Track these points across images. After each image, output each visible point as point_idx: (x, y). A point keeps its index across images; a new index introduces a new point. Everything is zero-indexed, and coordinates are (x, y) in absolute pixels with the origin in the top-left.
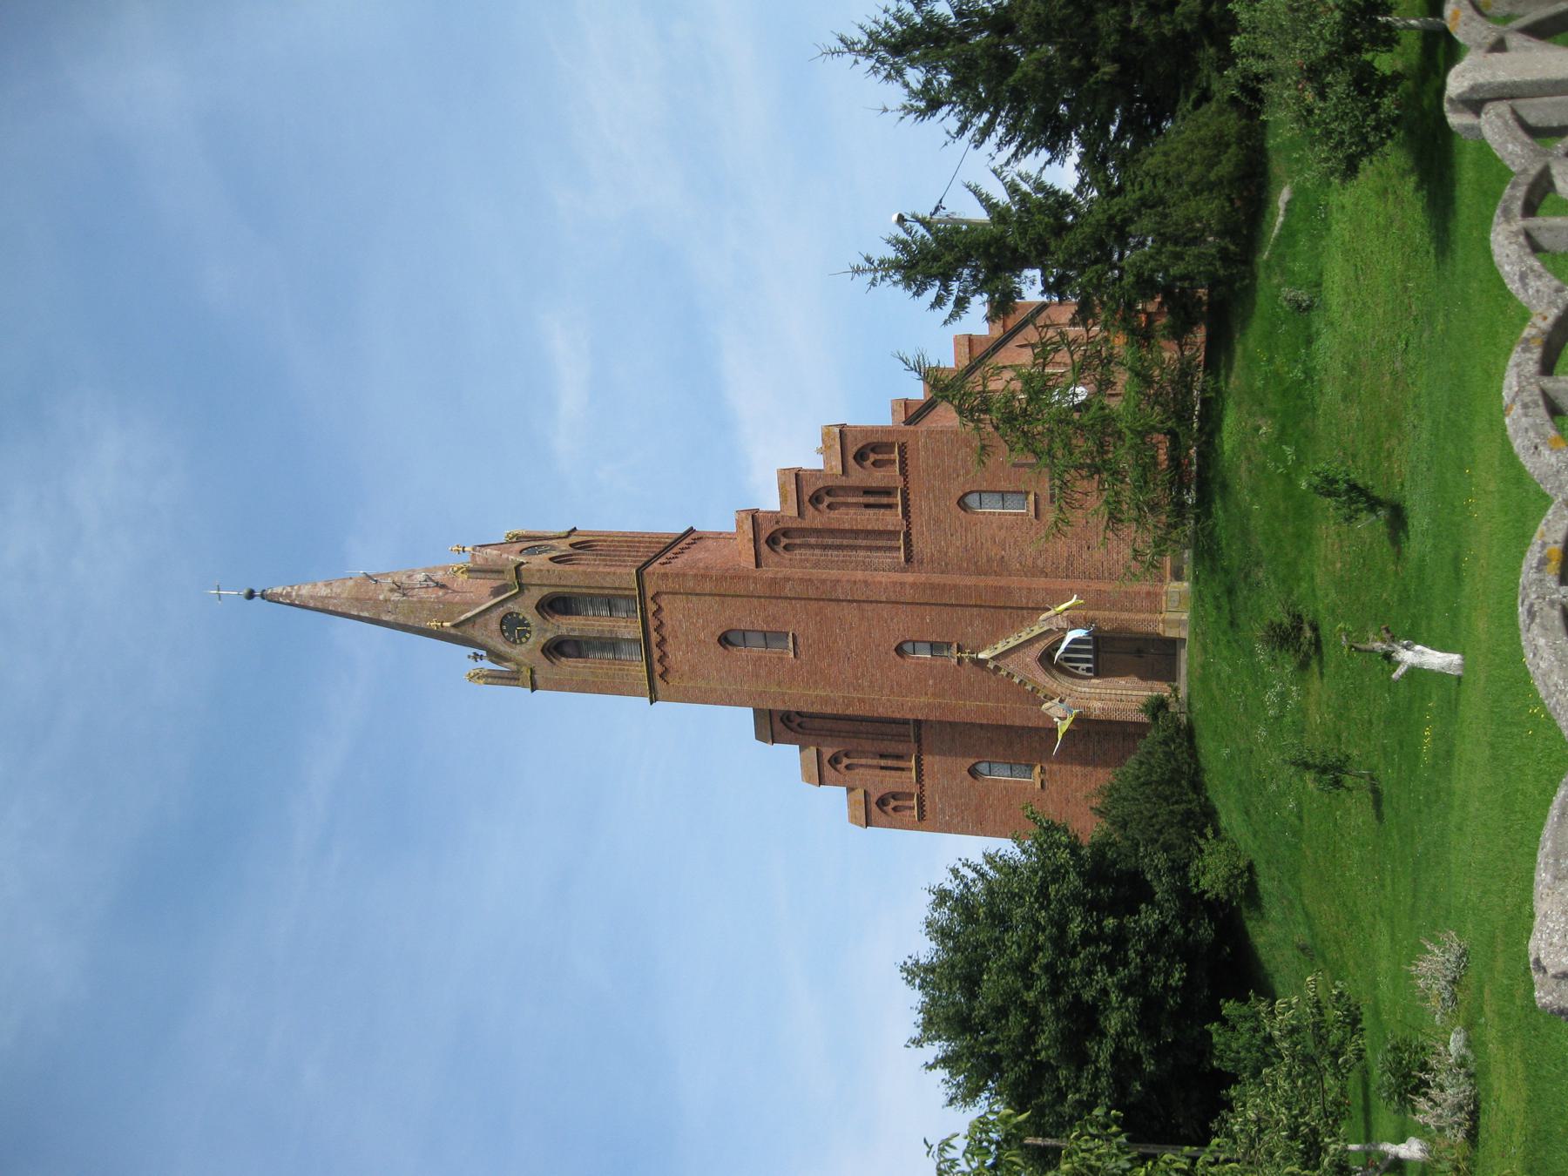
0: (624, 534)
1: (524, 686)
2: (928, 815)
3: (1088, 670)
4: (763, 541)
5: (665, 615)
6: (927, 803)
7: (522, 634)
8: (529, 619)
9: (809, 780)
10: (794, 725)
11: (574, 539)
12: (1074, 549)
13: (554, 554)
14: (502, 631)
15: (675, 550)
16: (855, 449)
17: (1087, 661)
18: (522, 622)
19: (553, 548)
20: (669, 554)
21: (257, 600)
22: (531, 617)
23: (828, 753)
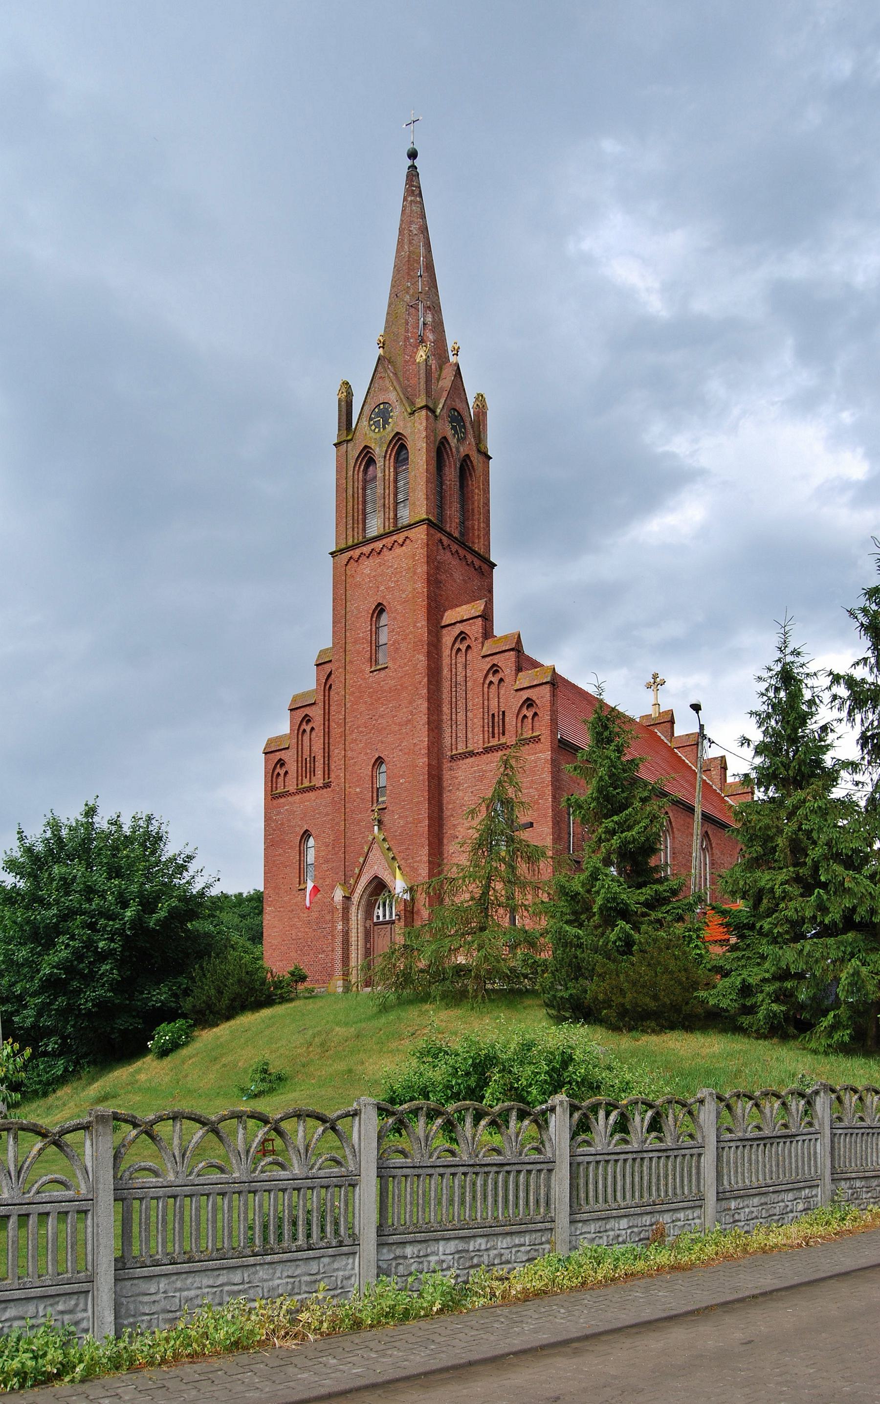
1: (339, 436)
2: (275, 802)
3: (378, 917)
4: (462, 628)
5: (398, 551)
7: (377, 424)
9: (294, 700)
11: (476, 458)
15: (462, 552)
16: (534, 698)
17: (384, 916)
18: (386, 422)
21: (409, 162)
23: (313, 712)
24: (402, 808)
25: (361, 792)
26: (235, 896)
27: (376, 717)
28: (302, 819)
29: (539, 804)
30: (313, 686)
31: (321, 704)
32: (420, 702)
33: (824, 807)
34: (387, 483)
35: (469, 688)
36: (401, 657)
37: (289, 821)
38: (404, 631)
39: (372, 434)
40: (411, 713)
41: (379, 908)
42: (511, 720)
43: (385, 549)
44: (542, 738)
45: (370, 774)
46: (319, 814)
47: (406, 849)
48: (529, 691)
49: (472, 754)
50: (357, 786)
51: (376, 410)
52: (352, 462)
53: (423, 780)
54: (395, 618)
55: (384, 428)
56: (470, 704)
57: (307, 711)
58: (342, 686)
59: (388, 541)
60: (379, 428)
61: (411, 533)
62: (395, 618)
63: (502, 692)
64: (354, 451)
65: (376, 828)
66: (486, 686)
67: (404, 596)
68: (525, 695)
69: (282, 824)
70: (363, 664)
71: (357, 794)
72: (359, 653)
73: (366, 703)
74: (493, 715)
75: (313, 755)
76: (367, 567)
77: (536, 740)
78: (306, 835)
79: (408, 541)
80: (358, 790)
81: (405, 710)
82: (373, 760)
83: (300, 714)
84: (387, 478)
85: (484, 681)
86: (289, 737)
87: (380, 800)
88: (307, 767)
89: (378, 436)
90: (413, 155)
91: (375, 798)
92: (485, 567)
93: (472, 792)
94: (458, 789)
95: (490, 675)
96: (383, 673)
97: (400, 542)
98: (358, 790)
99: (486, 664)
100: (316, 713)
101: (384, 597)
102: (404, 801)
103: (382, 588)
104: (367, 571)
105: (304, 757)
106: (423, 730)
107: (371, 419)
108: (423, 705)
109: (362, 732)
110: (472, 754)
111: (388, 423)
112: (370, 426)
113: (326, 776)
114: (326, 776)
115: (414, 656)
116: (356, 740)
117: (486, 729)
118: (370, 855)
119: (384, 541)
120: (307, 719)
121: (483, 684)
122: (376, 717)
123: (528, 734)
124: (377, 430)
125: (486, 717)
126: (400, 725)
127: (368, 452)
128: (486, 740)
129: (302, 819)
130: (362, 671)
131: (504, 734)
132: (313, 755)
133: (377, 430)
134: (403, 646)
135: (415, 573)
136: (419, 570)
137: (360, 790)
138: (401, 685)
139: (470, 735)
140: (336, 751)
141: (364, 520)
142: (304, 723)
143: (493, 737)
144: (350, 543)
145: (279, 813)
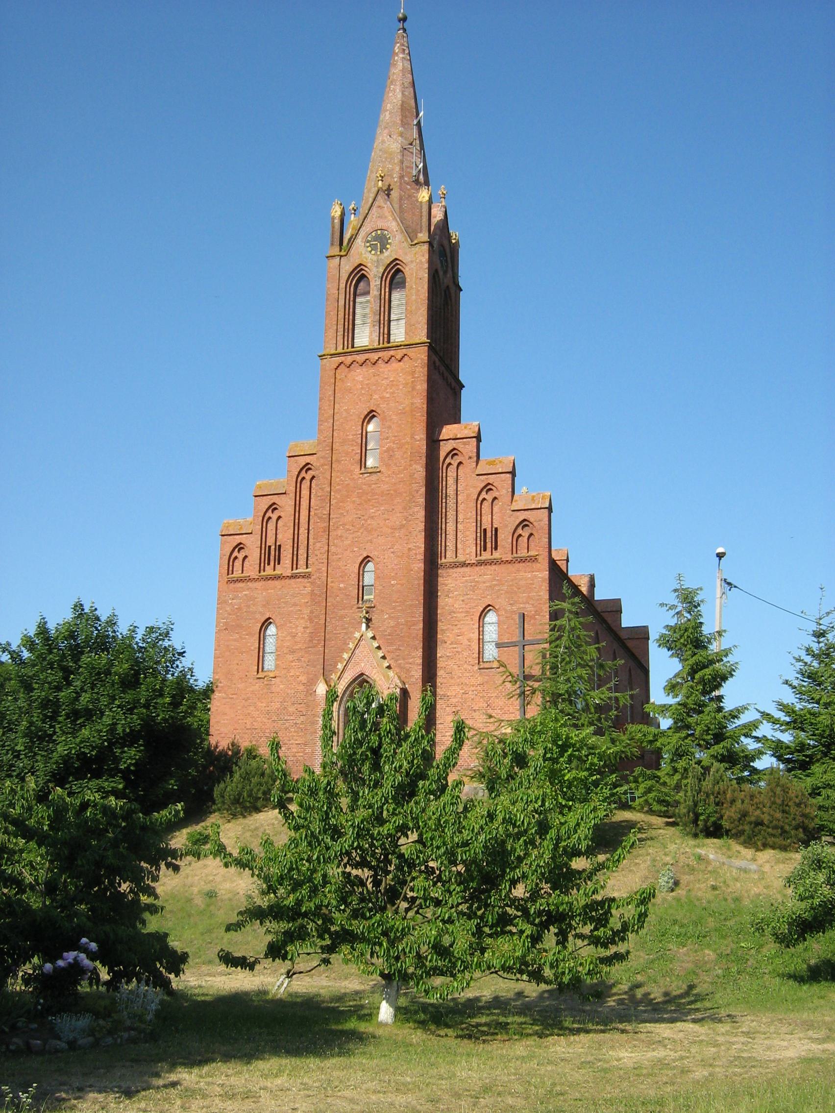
2: (232, 585)
4: (455, 446)
5: (394, 365)
6: (241, 585)
7: (374, 247)
8: (386, 253)
10: (484, 495)
11: (453, 289)
12: (454, 700)
13: (441, 273)
16: (532, 520)
18: (383, 248)
19: (445, 272)
20: (442, 369)
22: (388, 256)
24: (394, 608)
25: (345, 588)
26: (29, 644)
27: (366, 517)
29: (536, 619)
30: (283, 479)
31: (292, 495)
32: (416, 509)
34: (383, 301)
35: (459, 502)
36: (396, 464)
37: (248, 606)
38: (400, 440)
39: (368, 254)
40: (406, 519)
42: (505, 538)
43: (380, 361)
44: (540, 558)
45: (357, 571)
46: (285, 603)
47: (396, 649)
48: (526, 512)
49: (464, 565)
50: (342, 582)
51: (373, 234)
52: (344, 276)
53: (419, 584)
54: (390, 427)
55: (381, 252)
56: (460, 517)
57: (275, 499)
58: (327, 482)
59: (374, 356)
61: (411, 352)
62: (390, 427)
63: (495, 509)
65: (364, 625)
66: (479, 502)
68: (238, 539)
69: (239, 609)
70: (352, 465)
71: (340, 589)
72: (347, 453)
73: (354, 502)
74: (485, 530)
75: (278, 544)
76: (359, 375)
77: (534, 559)
78: (267, 623)
80: (342, 585)
81: (398, 515)
82: (361, 559)
84: (383, 296)
85: (477, 499)
87: (365, 597)
88: (271, 555)
91: (361, 595)
94: (447, 596)
95: (484, 493)
96: (374, 477)
97: (399, 357)
98: (342, 585)
99: (481, 483)
100: (286, 504)
101: (378, 405)
103: (376, 397)
104: (360, 378)
105: (268, 544)
106: (419, 537)
108: (420, 514)
109: (348, 530)
110: (464, 565)
113: (295, 566)
114: (295, 566)
115: (411, 465)
117: (479, 542)
118: (357, 651)
119: (380, 354)
120: (273, 507)
121: (477, 499)
122: (366, 517)
123: (523, 553)
125: (479, 531)
126: (393, 529)
127: (399, 271)
128: (479, 552)
129: (264, 606)
130: (351, 472)
131: (496, 548)
132: (278, 544)
134: (398, 454)
135: (413, 389)
136: (419, 387)
137: (344, 586)
139: (459, 546)
142: (270, 511)
144: (340, 350)
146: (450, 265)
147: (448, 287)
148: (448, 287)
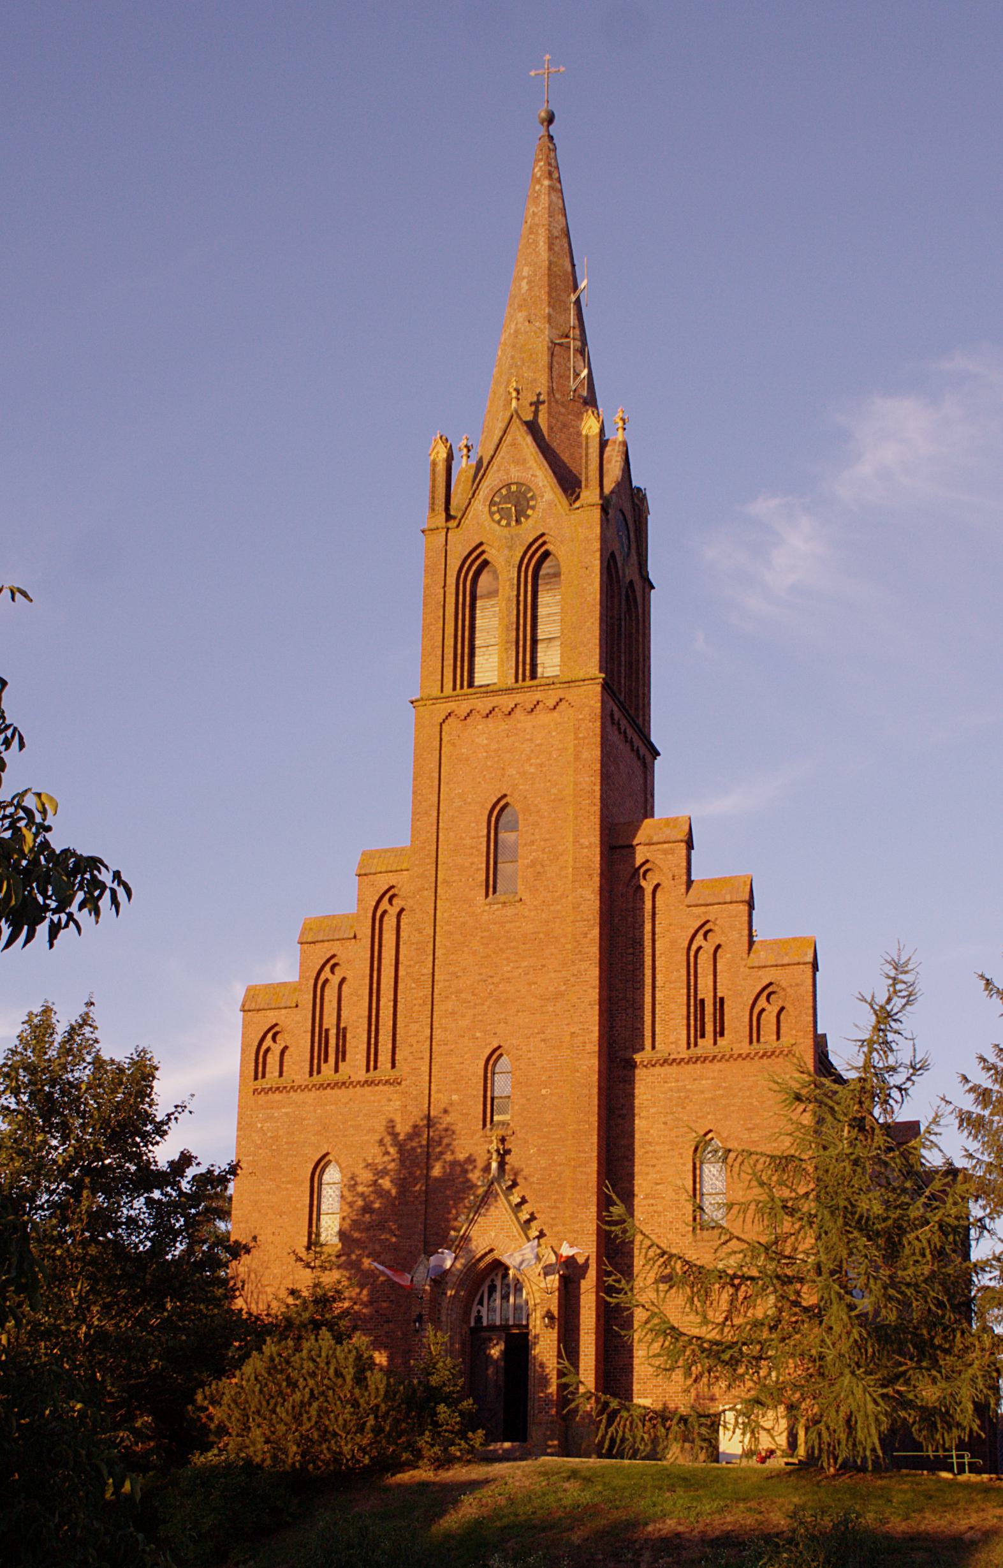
0: (601, 629)
5: (543, 717)
6: (277, 1096)
11: (638, 587)
14: (509, 485)
18: (521, 515)
22: (528, 530)
27: (496, 980)
28: (319, 1133)
32: (584, 966)
33: (150, 1147)
41: (481, 1303)
43: (518, 710)
50: (457, 1091)
51: (504, 491)
55: (518, 521)
57: (336, 948)
60: (509, 519)
61: (571, 695)
64: (459, 549)
67: (554, 791)
69: (276, 1138)
73: (475, 953)
79: (563, 705)
81: (553, 975)
83: (320, 954)
86: (295, 988)
87: (496, 1118)
88: (326, 1046)
89: (506, 530)
90: (550, 119)
92: (649, 757)
93: (665, 1123)
102: (549, 1125)
103: (512, 771)
107: (492, 503)
109: (465, 1001)
111: (528, 517)
112: (491, 514)
116: (453, 1013)
122: (496, 980)
124: (504, 522)
129: (319, 1133)
132: (342, 1025)
133: (504, 522)
136: (585, 755)
138: (547, 934)
140: (414, 1027)
141: (472, 655)
143: (703, 1036)
145: (270, 1118)
146: (634, 545)
147: (631, 582)
148: (631, 582)
